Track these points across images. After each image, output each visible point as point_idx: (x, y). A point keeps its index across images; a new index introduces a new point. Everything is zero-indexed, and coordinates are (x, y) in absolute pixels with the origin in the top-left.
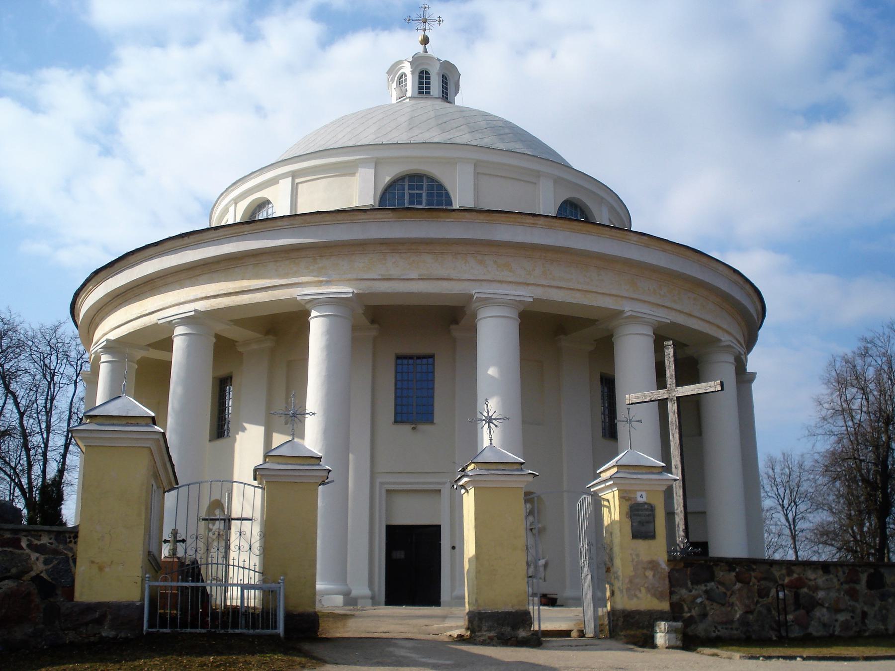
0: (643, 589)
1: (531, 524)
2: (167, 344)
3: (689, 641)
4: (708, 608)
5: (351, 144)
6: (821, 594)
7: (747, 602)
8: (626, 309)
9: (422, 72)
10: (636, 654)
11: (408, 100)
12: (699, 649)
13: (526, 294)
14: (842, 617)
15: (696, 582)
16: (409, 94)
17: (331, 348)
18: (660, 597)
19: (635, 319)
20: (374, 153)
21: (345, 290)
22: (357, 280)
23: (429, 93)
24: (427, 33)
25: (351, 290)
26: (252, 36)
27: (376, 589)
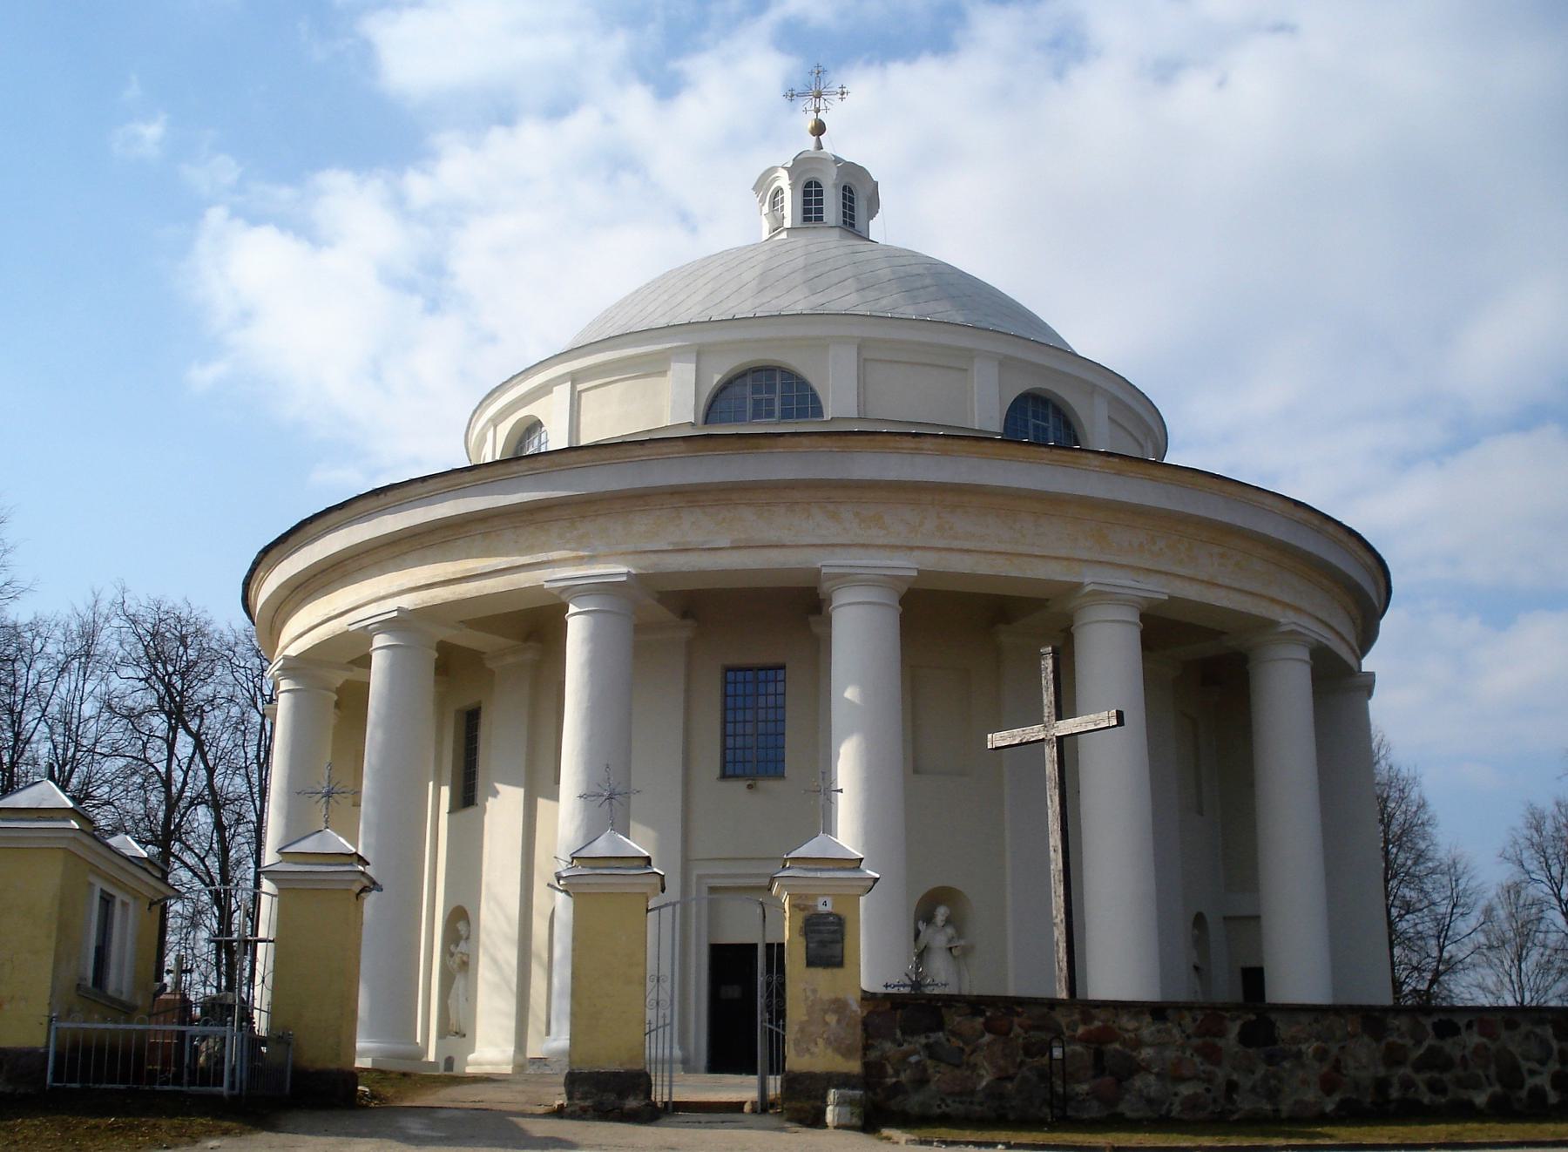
0: (820, 1041)
1: (950, 941)
2: (365, 662)
3: (871, 1120)
4: (930, 1071)
5: (662, 323)
6: (1146, 1053)
7: (1002, 1062)
8: (1087, 580)
9: (809, 185)
10: (785, 1136)
11: (784, 235)
12: (886, 1132)
13: (906, 565)
14: (1186, 1090)
15: (910, 1031)
16: (788, 223)
17: (595, 663)
18: (847, 1053)
19: (1102, 596)
20: (694, 338)
21: (616, 569)
22: (636, 552)
23: (821, 219)
24: (821, 116)
25: (624, 570)
26: (667, 88)
27: (692, 1048)
